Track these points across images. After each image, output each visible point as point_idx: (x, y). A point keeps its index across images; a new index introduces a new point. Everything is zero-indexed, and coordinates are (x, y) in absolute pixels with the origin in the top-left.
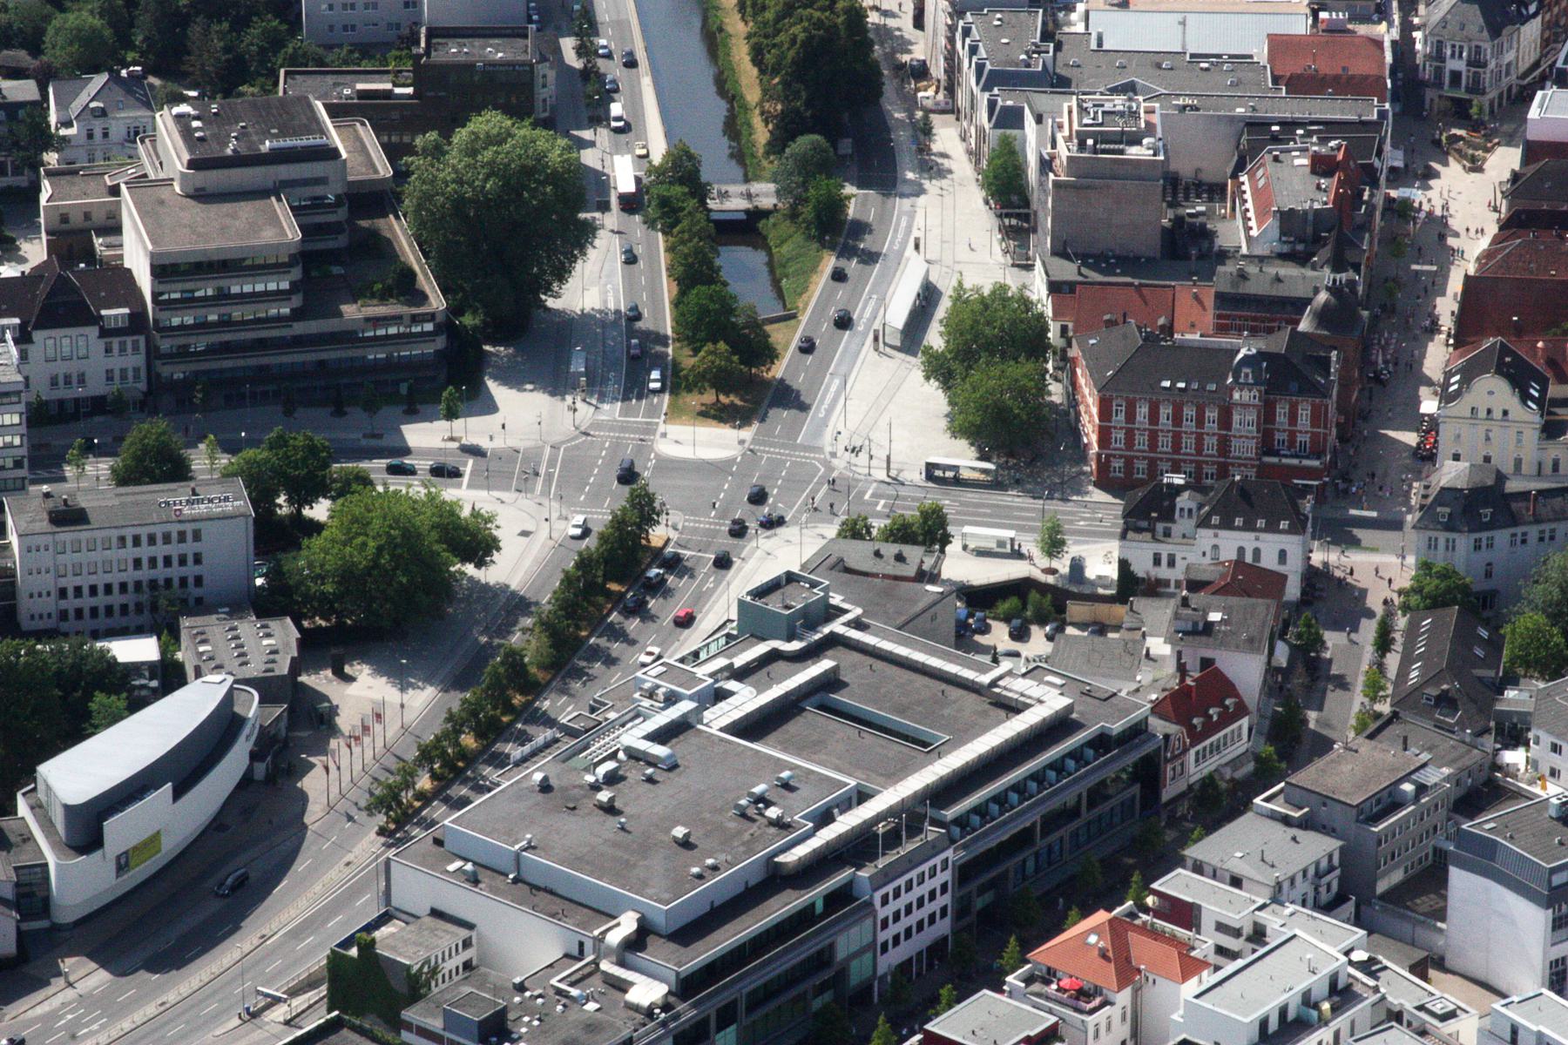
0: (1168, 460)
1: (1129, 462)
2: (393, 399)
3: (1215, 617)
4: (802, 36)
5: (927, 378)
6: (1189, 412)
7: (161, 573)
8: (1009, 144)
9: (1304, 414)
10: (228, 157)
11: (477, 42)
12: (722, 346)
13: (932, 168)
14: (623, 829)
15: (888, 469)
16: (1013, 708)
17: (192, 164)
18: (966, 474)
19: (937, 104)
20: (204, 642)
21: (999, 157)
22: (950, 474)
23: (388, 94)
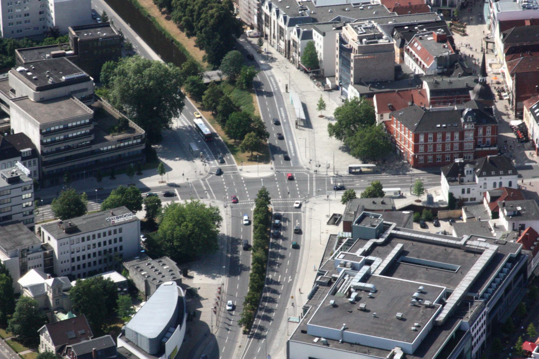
0: (431, 155)
1: (434, 156)
3: (519, 208)
5: (331, 135)
6: (448, 135)
7: (108, 247)
9: (489, 129)
10: (51, 85)
11: (92, 30)
14: (375, 317)
16: (479, 252)
17: (38, 89)
18: (364, 170)
20: (142, 270)
22: (358, 170)
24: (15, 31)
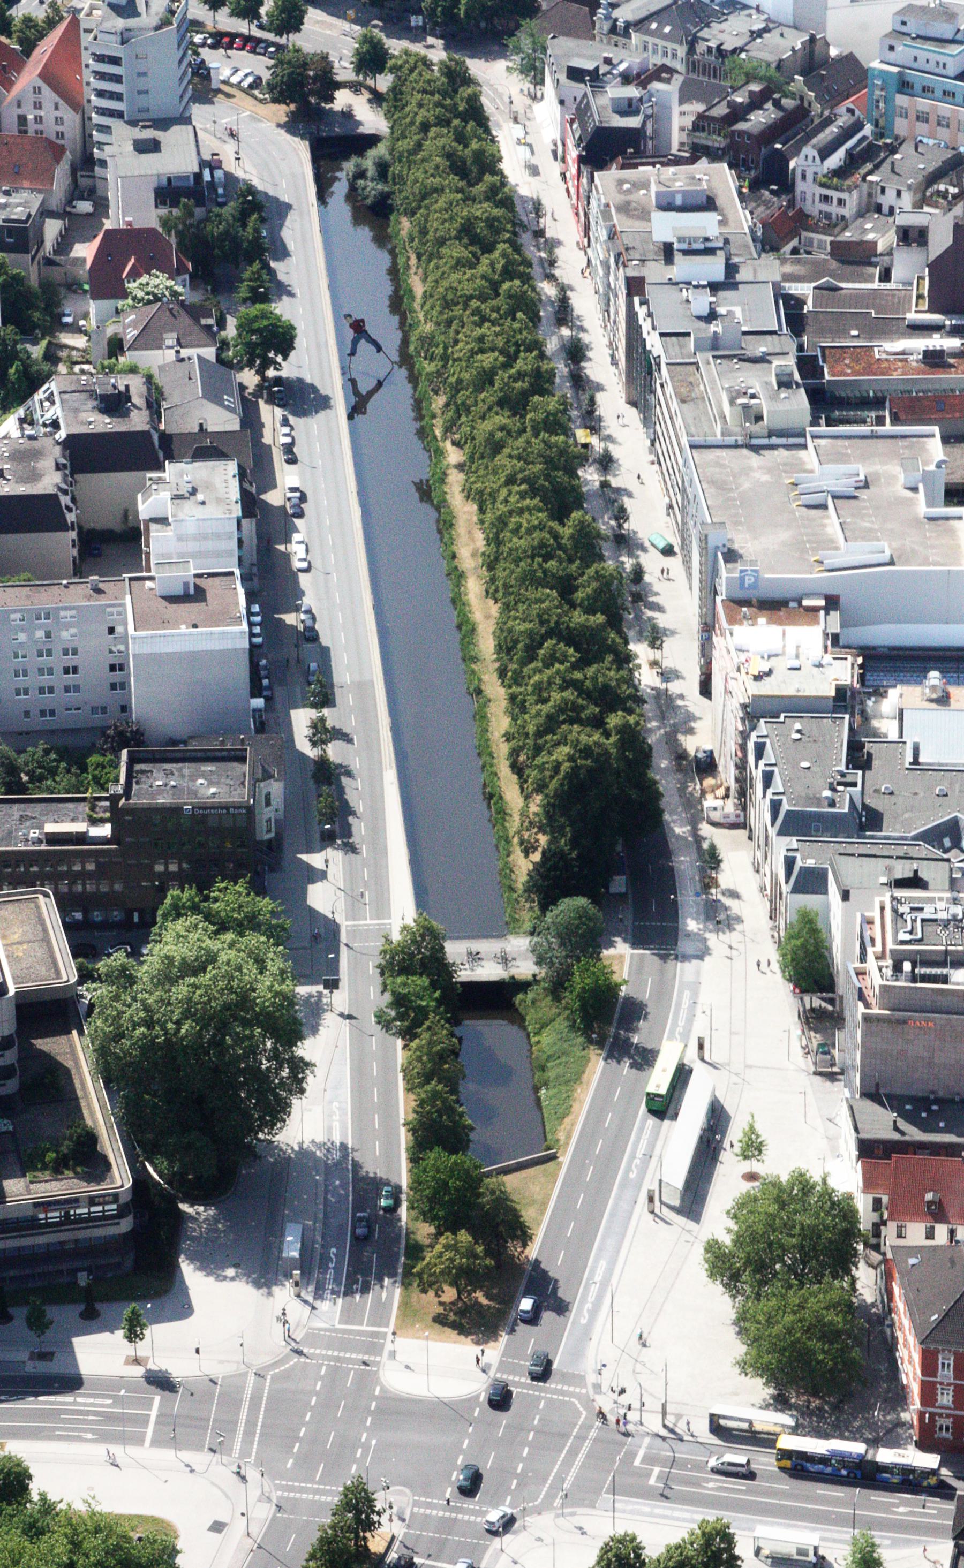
2: (64, 1293)
4: (565, 767)
8: (811, 921)
12: (464, 1237)
13: (718, 917)
15: (664, 1413)
19: (726, 816)
21: (797, 937)
23: (81, 838)
24: (35, 713)
